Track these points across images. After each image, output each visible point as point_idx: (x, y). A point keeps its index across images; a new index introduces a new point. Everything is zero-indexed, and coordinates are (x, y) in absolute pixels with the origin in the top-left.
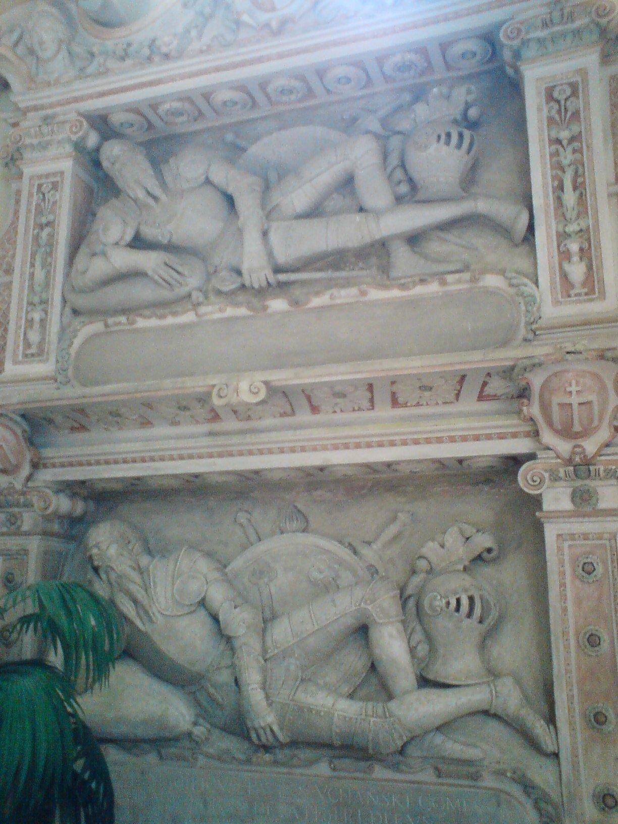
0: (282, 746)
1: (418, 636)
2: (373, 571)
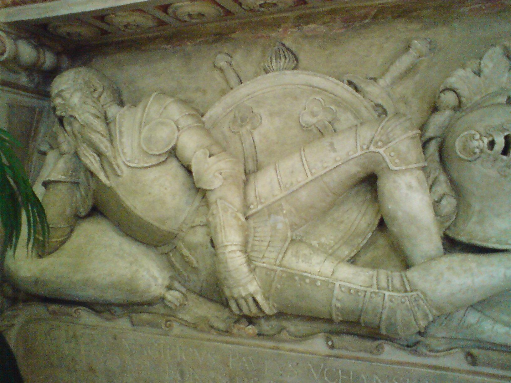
0: (268, 318)
1: (443, 187)
2: (381, 111)
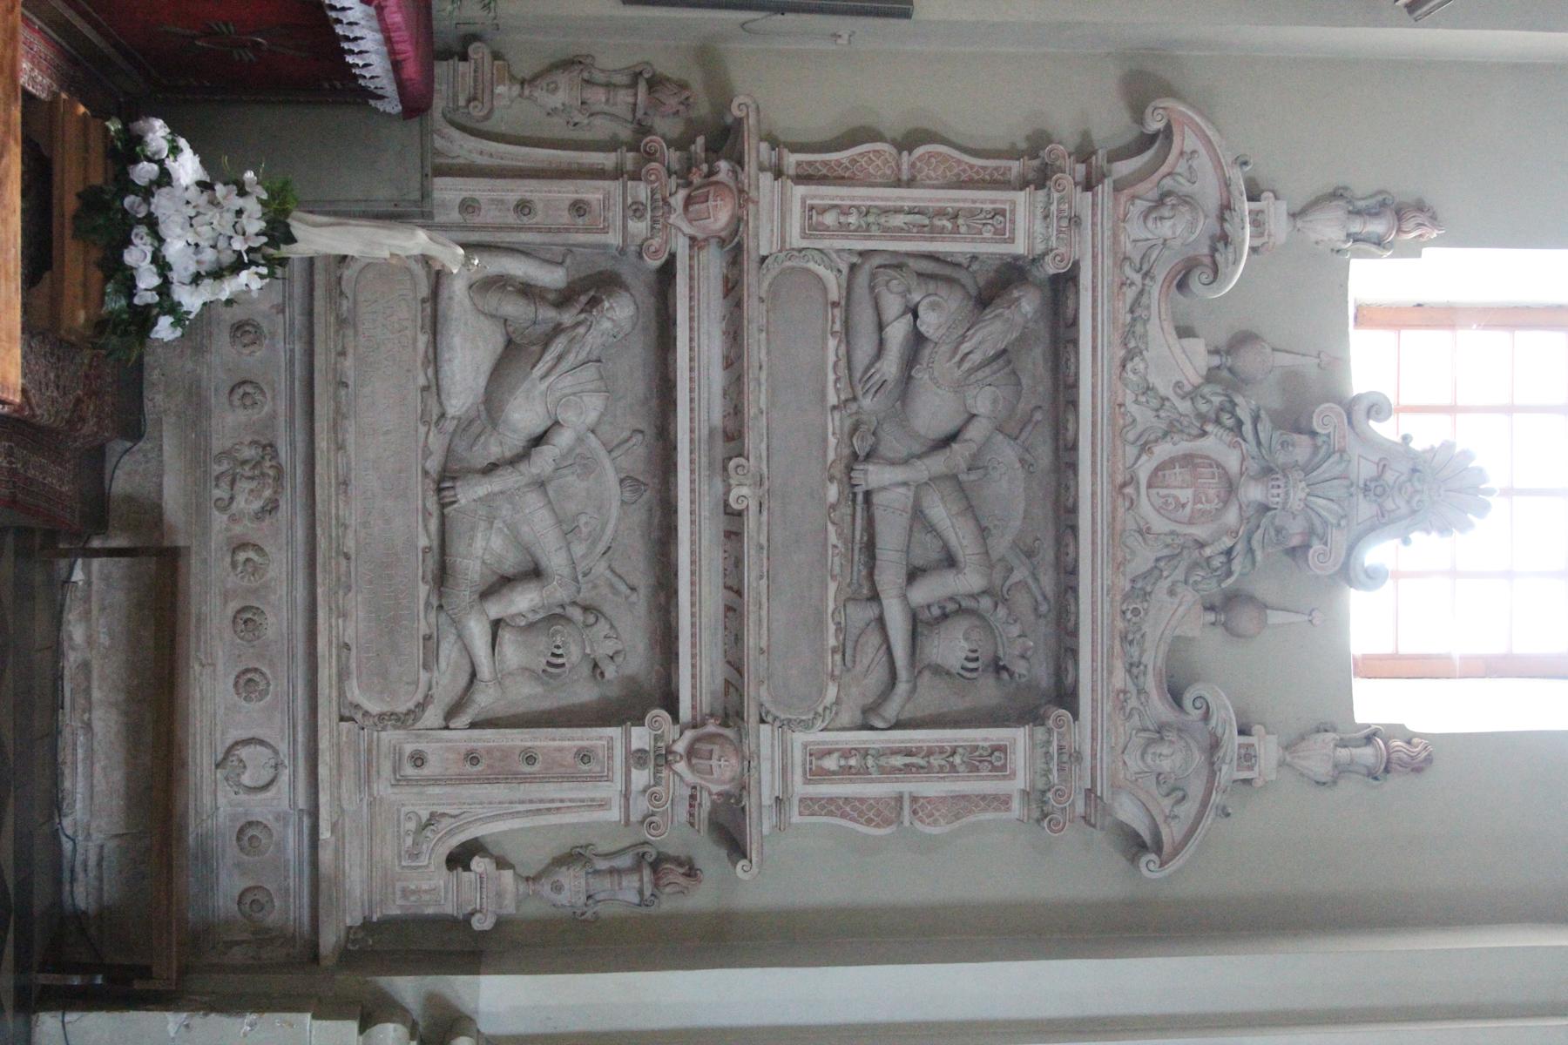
1: (532, 618)
